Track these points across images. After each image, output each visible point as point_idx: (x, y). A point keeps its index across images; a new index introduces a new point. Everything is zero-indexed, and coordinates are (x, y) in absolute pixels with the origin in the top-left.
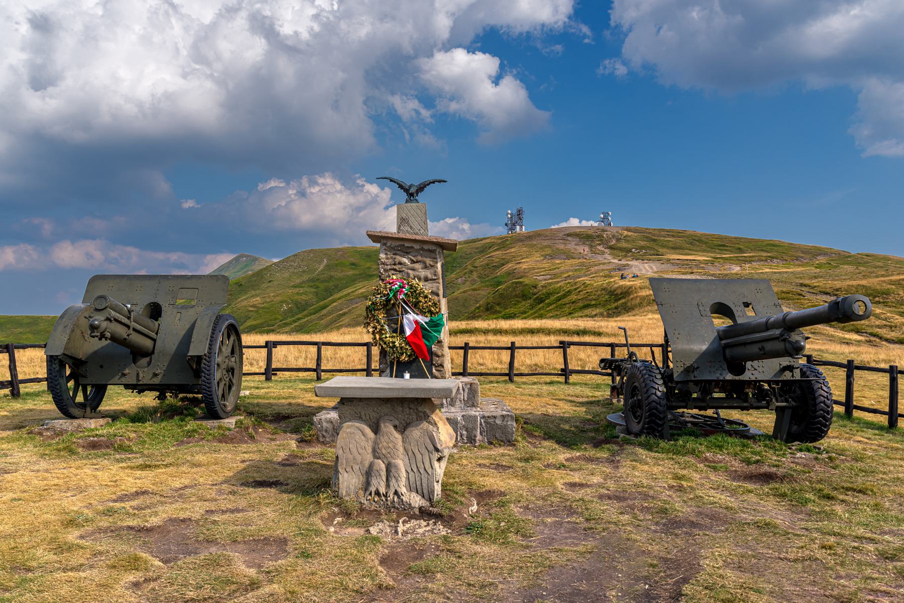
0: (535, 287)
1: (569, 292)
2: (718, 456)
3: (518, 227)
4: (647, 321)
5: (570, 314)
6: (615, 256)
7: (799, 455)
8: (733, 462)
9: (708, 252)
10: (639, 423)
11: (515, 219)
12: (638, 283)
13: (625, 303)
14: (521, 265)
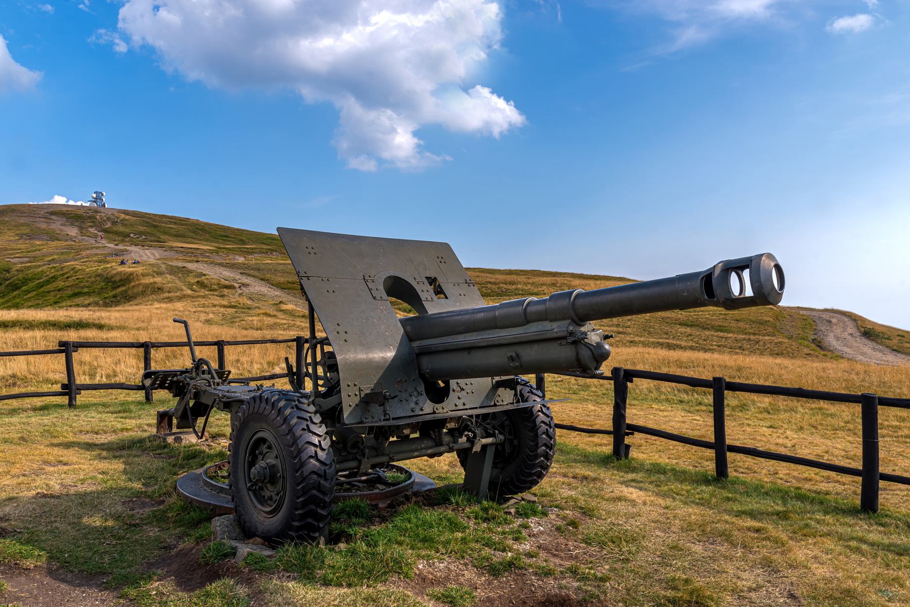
0: (8, 271)
1: (54, 278)
4: (155, 311)
5: (56, 303)
6: (111, 241)
9: (212, 241)
12: (139, 269)
13: (126, 291)
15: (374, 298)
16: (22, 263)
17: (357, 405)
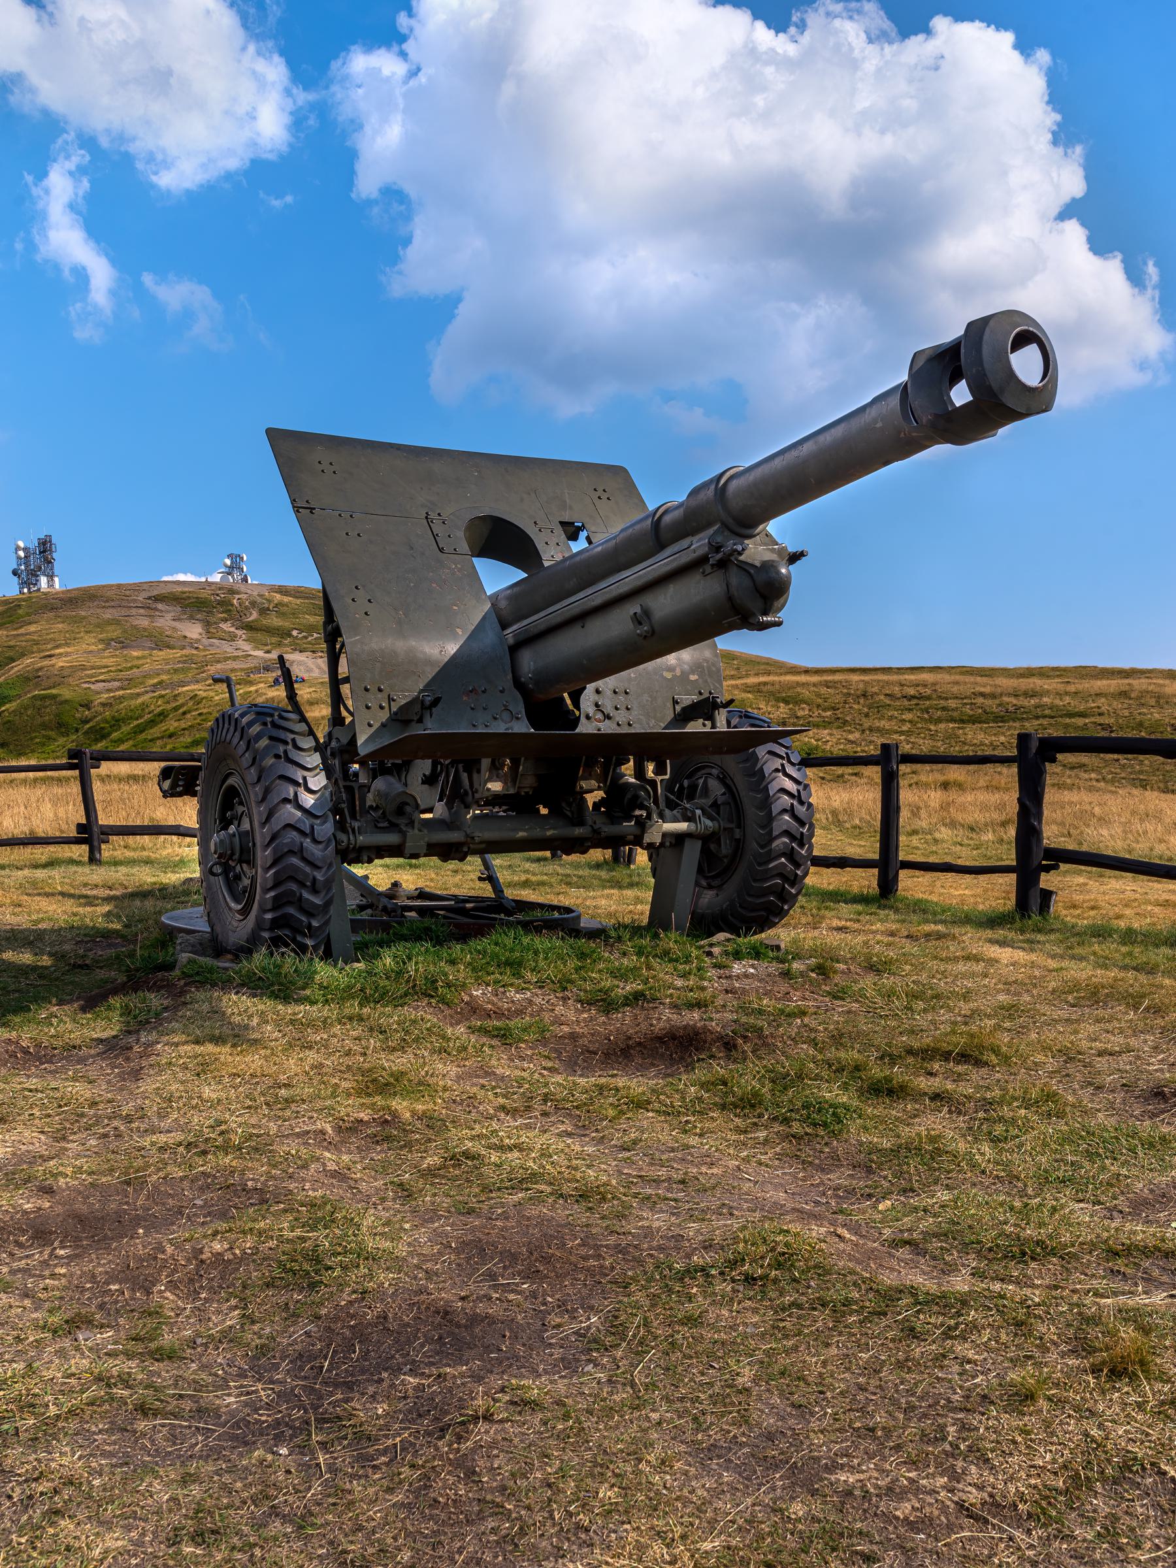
0: (87, 706)
1: (163, 715)
2: (511, 993)
3: (43, 581)
6: (258, 644)
7: (737, 968)
8: (560, 1009)
10: (245, 912)
11: (34, 562)
14: (54, 661)
15: (441, 550)
16: (109, 691)
17: (383, 725)
